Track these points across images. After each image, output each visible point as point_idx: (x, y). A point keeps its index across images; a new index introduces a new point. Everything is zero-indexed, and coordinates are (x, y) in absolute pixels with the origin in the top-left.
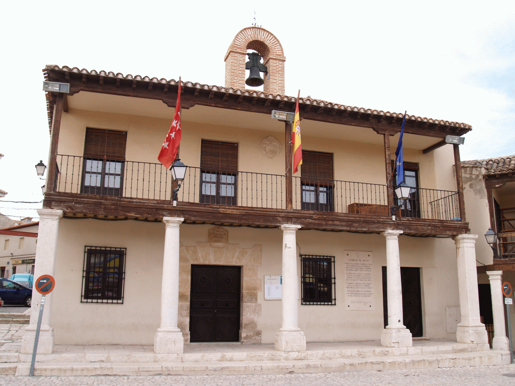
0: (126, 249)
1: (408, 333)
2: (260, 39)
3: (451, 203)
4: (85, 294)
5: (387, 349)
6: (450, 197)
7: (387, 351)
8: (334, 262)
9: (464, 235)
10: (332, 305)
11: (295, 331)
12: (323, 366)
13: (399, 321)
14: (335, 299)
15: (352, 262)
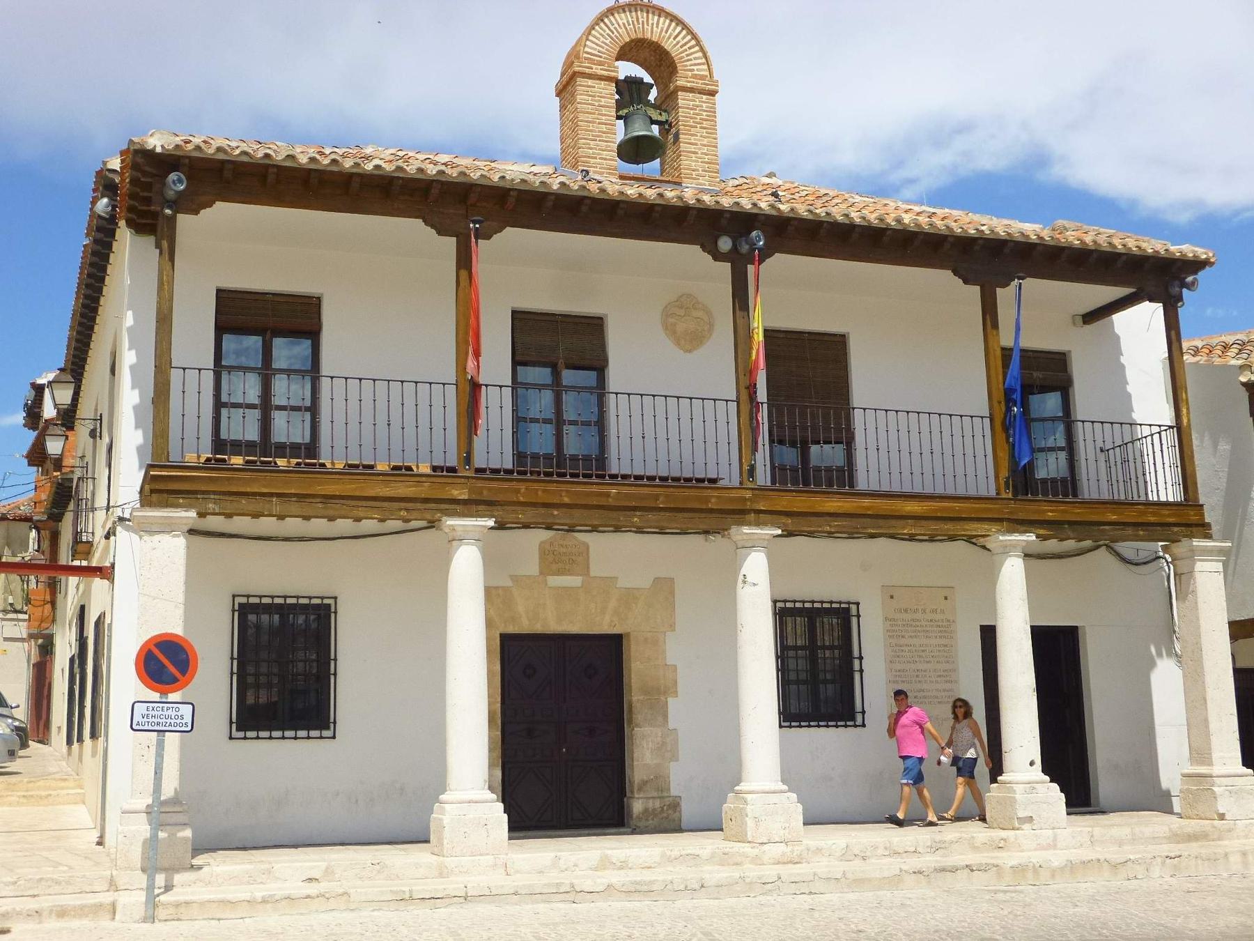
0: (335, 598)
1: (1054, 795)
2: (648, 36)
3: (1158, 454)
4: (852, 679)
5: (1003, 834)
6: (1156, 437)
7: (1005, 840)
8: (858, 616)
9: (1196, 542)
10: (856, 726)
11: (774, 792)
12: (849, 875)
13: (1032, 764)
14: (863, 712)
15: (905, 616)
